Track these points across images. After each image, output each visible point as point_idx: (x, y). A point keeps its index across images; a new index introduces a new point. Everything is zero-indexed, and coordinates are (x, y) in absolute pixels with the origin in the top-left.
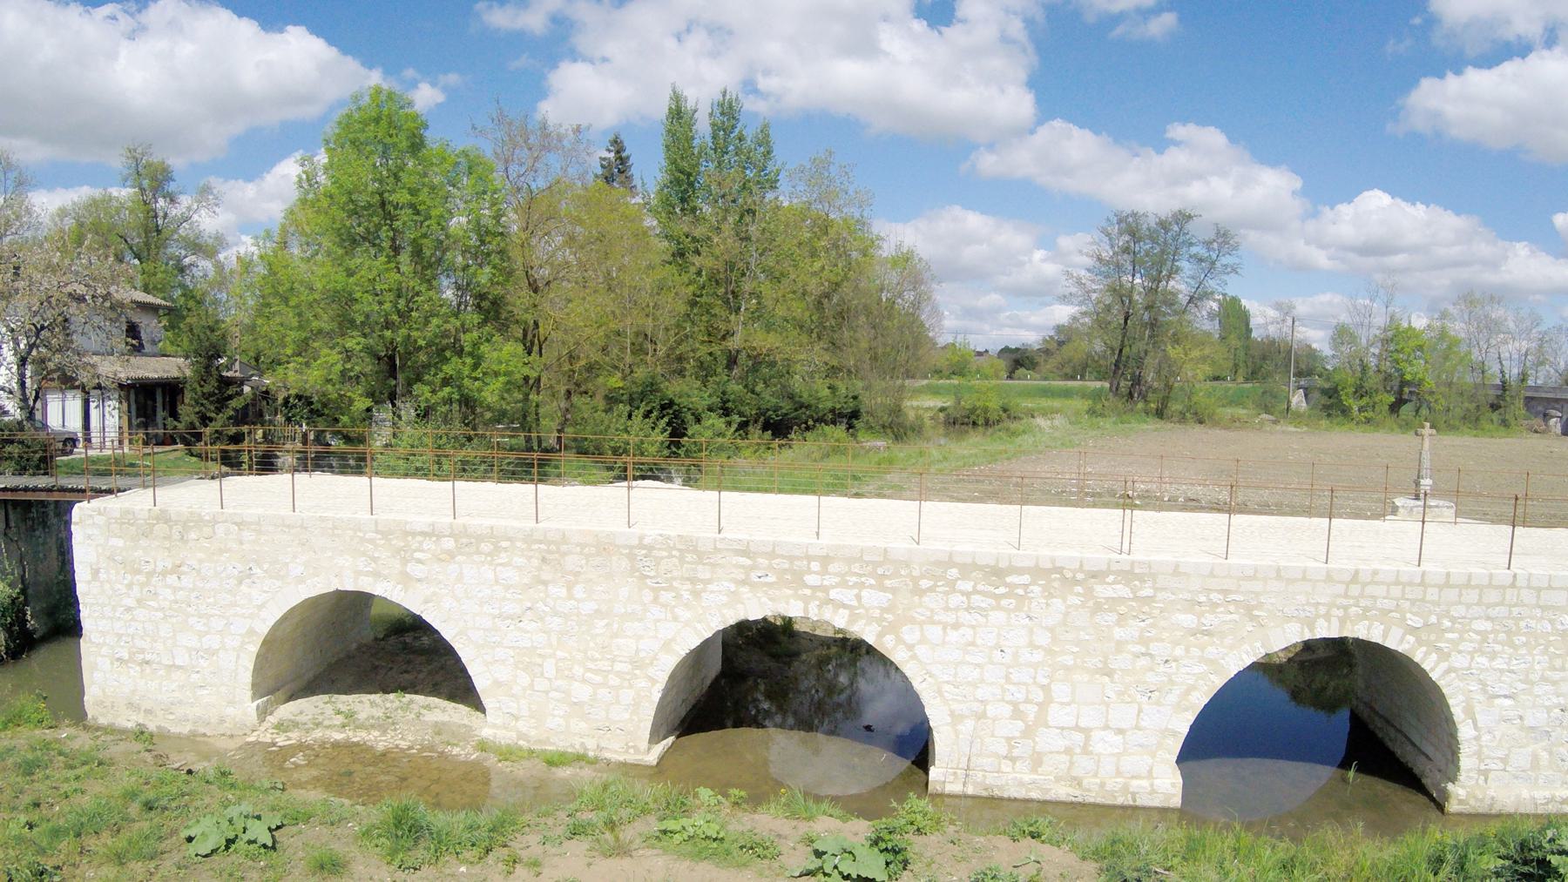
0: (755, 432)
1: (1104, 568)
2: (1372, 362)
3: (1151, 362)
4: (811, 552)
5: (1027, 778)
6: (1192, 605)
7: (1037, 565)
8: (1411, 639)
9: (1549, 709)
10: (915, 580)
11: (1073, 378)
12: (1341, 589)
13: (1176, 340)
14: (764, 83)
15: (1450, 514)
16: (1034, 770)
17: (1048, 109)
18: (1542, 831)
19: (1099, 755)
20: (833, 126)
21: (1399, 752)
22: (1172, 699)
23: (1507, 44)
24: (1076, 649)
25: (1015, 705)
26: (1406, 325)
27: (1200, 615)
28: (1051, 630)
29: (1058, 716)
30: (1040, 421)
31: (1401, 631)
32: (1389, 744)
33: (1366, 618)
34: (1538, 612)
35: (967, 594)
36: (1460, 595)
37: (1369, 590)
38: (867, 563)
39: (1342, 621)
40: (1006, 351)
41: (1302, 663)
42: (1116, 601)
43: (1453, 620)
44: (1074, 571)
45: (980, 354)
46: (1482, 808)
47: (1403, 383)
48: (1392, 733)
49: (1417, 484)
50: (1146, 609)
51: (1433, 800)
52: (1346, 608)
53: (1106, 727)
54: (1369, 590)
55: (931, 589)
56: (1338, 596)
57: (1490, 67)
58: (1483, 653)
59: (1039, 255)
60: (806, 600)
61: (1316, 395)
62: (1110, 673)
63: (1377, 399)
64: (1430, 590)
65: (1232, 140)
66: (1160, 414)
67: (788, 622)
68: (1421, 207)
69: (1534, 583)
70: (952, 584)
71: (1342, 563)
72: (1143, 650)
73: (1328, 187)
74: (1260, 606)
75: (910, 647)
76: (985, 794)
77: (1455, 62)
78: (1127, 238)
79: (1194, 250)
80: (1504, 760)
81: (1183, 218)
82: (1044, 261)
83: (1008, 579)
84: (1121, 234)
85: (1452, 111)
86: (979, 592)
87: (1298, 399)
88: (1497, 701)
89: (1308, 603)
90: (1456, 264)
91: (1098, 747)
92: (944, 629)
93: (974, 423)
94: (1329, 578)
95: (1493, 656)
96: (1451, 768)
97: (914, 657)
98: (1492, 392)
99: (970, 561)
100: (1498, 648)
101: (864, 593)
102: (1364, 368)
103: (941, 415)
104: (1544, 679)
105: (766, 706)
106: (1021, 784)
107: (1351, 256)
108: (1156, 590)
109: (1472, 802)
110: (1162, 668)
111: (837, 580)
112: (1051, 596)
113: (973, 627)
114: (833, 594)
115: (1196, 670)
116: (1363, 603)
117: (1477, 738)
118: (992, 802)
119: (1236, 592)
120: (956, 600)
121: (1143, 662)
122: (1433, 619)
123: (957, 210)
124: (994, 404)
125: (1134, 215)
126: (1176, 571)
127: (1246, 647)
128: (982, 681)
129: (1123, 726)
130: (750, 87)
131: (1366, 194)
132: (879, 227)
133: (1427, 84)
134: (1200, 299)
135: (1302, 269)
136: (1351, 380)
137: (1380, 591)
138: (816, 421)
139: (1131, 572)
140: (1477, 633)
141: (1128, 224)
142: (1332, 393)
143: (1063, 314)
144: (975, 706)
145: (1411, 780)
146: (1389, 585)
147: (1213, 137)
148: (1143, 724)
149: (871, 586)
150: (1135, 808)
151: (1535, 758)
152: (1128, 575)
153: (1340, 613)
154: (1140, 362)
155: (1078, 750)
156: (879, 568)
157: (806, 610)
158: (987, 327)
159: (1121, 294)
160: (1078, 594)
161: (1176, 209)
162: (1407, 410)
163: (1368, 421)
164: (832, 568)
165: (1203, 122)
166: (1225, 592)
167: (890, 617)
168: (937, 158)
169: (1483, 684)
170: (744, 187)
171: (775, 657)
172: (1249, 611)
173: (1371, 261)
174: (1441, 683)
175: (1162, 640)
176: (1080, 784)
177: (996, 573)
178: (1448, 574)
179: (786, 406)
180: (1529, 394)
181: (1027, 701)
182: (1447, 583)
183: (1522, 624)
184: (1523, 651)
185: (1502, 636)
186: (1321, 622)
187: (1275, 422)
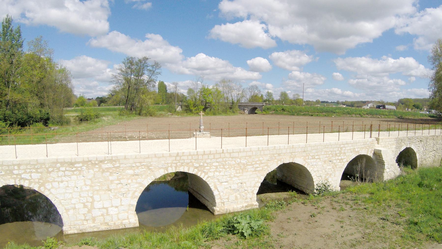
0: (16, 127)
1: (104, 159)
2: (198, 97)
3: (136, 100)
4: (14, 163)
5: (92, 225)
6: (131, 167)
7: (83, 160)
8: (196, 170)
9: (237, 184)
10: (47, 169)
11: (117, 105)
12: (174, 158)
13: (143, 93)
14: (28, 15)
15: (209, 135)
16: (94, 222)
17: (112, 28)
18: (233, 217)
19: (112, 215)
20: (48, 30)
21: (201, 200)
22: (130, 195)
23: (238, 18)
24: (99, 184)
25: (84, 203)
26: (206, 87)
27: (134, 170)
28: (91, 179)
29: (97, 205)
30: (104, 118)
31: (193, 168)
32: (198, 199)
33: (183, 166)
34: (231, 159)
35: (64, 171)
36: (208, 157)
37: (182, 158)
38: (32, 165)
39: (176, 167)
40: (98, 98)
41: (175, 180)
42: (108, 169)
43: (207, 163)
44: (95, 161)
45: (89, 99)
46: (224, 212)
47: (206, 103)
48: (199, 196)
49: (200, 128)
50: (118, 170)
51: (211, 212)
52: (176, 163)
53: (112, 206)
54: (182, 158)
55: (53, 171)
56: (174, 160)
58: (217, 172)
59: (108, 70)
60: (15, 179)
61: (184, 107)
62: (110, 190)
63: (199, 107)
64: (200, 156)
65: (164, 38)
66: (140, 114)
67: (22, 186)
68: (214, 58)
69: (228, 151)
70: (59, 169)
71: (174, 151)
72: (119, 182)
73: (189, 52)
74: (151, 165)
75: (49, 190)
76: (81, 232)
77: (224, 22)
78: (130, 64)
79: (148, 68)
80: (228, 199)
81: (146, 59)
82: (109, 72)
83: (76, 165)
84: (128, 63)
86: (67, 170)
87: (179, 109)
88: (223, 184)
89: (165, 163)
90: (222, 73)
91: (111, 213)
92: (59, 183)
93: (87, 120)
94: (170, 156)
95: (220, 172)
96: (214, 204)
97: (51, 193)
98: (230, 104)
99: (63, 161)
100: (221, 169)
101: (32, 175)
102: (196, 99)
103: (77, 118)
104: (235, 176)
105: (30, 214)
106: (91, 227)
107: (196, 71)
108: (120, 164)
109: (221, 211)
110: (125, 187)
111: (24, 171)
112: (89, 169)
113: (67, 181)
114: (23, 176)
115: (136, 186)
116: (181, 162)
117: (219, 194)
118: (83, 234)
119: (144, 162)
120: (61, 173)
121: (119, 186)
122: (202, 164)
123: (85, 57)
124: (93, 114)
125: (131, 58)
126: (125, 158)
127: (149, 178)
128: (73, 198)
129: (117, 205)
130: (23, 15)
131: (199, 54)
132: (55, 60)
133: (217, 27)
134: (150, 81)
135: (182, 74)
136: (192, 102)
137: (185, 158)
138: (33, 121)
139: (112, 160)
140: (214, 166)
141: (130, 61)
142: (187, 106)
143: (111, 87)
144: (73, 206)
145: (204, 207)
146: (188, 156)
147: (159, 38)
148: (123, 204)
149: (34, 172)
150: (126, 229)
151: (236, 197)
152: (111, 161)
153: (175, 165)
154: (133, 99)
155: (105, 214)
156: (36, 166)
157: (15, 182)
158: (93, 91)
159: (128, 81)
160: (97, 168)
161: (144, 56)
162: (207, 110)
164: (22, 167)
165: (155, 33)
166: (141, 163)
167: (41, 181)
168: (78, 41)
169: (218, 180)
170: (12, 47)
171: (17, 198)
172: (148, 167)
173: (200, 72)
174: (206, 181)
175: (124, 179)
176: (108, 224)
177: (72, 164)
178: (204, 151)
179: (25, 117)
180: (240, 104)
181: (87, 202)
182: (204, 154)
183: (227, 163)
184: (228, 170)
185: (222, 166)
186: (170, 168)
187: (172, 115)
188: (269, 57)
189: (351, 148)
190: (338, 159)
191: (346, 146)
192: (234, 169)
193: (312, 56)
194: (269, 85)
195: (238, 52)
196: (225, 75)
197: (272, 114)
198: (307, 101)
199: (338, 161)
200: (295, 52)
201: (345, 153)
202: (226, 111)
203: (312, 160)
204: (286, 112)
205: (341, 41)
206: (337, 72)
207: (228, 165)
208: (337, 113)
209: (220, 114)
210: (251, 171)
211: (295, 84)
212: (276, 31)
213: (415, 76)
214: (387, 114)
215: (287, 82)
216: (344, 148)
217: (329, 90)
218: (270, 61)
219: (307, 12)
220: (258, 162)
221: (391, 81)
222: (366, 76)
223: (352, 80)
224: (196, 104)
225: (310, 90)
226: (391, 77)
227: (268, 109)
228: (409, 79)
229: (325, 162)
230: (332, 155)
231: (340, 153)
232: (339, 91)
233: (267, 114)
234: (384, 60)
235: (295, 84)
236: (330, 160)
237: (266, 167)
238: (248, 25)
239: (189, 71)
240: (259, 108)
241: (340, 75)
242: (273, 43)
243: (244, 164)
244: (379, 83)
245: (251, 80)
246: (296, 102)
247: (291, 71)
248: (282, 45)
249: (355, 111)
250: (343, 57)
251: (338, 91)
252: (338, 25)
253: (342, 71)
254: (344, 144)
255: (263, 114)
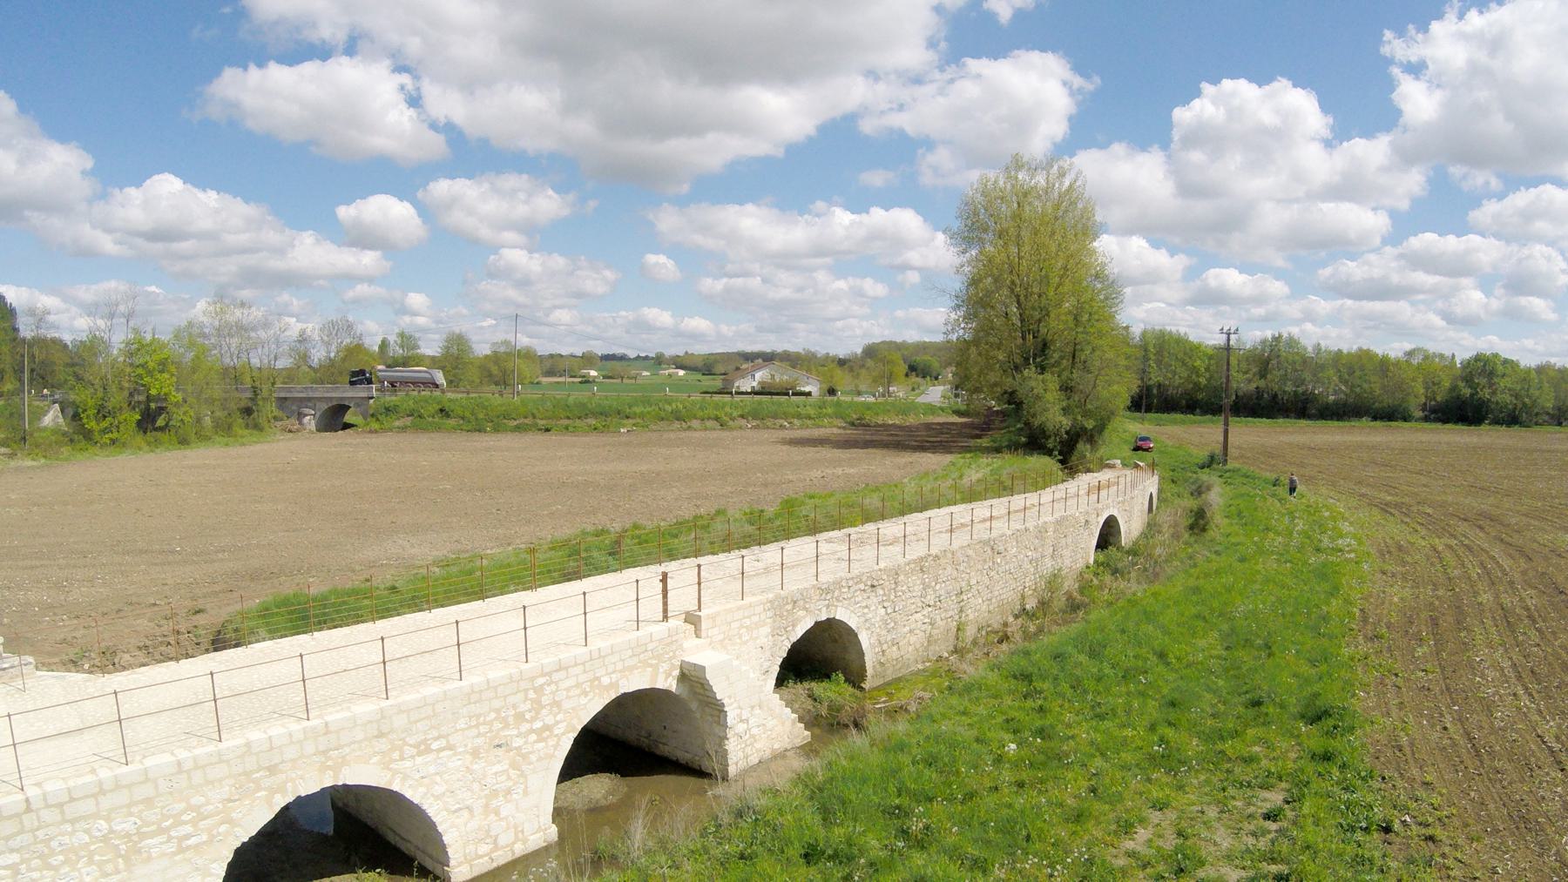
26: (149, 337)
34: (68, 827)
57: (290, 65)
65: (23, 109)
68: (213, 194)
73: (119, 168)
85: (250, 101)
90: (244, 251)
107: (140, 242)
131: (156, 177)
133: (229, 74)
135: (86, 254)
163: (113, 442)
180: (283, 395)
183: (54, 844)
185: (36, 863)
188: (420, 194)
189: (582, 678)
190: (532, 731)
191: (556, 677)
192: (91, 862)
193: (571, 197)
194: (416, 300)
195: (307, 174)
196: (252, 260)
197: (403, 429)
198: (552, 356)
199: (533, 737)
200: (511, 181)
201: (557, 704)
202: (230, 427)
203: (419, 760)
204: (452, 422)
205: (676, 147)
206: (657, 253)
207: (61, 852)
208: (635, 416)
209: (202, 437)
210: (164, 854)
211: (512, 293)
212: (447, 104)
213: (919, 269)
214: (812, 412)
215: (483, 286)
216: (553, 687)
217: (631, 316)
218: (422, 209)
219: (565, 42)
220: (185, 818)
221: (841, 284)
222: (756, 267)
223: (708, 282)
224: (110, 406)
225: (563, 316)
226: (839, 271)
227: (387, 409)
228: (900, 278)
229: (475, 754)
230: (505, 721)
231: (538, 706)
232: (664, 318)
233: (384, 430)
234: (818, 215)
235: (512, 293)
236: (497, 742)
237: (223, 828)
238: (347, 73)
239: (117, 242)
240: (358, 405)
241: (670, 264)
242: (436, 144)
243: (128, 835)
244: (800, 289)
245: (351, 278)
246: (500, 370)
247: (496, 248)
248: (470, 154)
249: (701, 408)
250: (682, 202)
251: (662, 317)
252: (670, 92)
253: (676, 251)
254: (549, 674)
255: (371, 432)
